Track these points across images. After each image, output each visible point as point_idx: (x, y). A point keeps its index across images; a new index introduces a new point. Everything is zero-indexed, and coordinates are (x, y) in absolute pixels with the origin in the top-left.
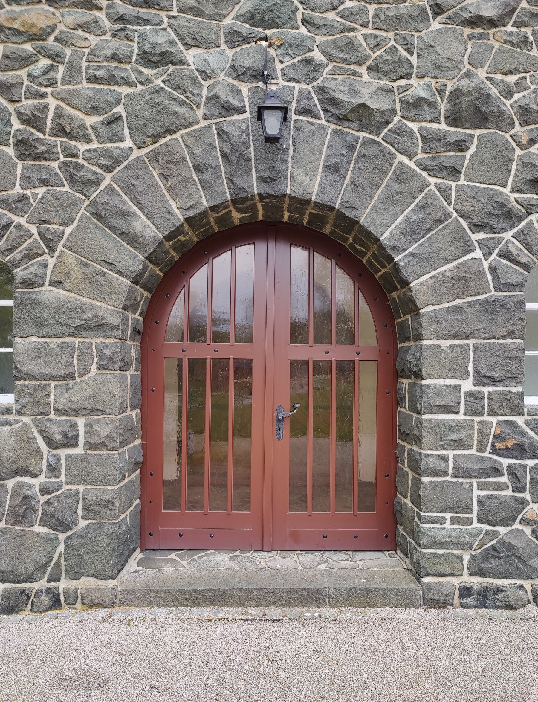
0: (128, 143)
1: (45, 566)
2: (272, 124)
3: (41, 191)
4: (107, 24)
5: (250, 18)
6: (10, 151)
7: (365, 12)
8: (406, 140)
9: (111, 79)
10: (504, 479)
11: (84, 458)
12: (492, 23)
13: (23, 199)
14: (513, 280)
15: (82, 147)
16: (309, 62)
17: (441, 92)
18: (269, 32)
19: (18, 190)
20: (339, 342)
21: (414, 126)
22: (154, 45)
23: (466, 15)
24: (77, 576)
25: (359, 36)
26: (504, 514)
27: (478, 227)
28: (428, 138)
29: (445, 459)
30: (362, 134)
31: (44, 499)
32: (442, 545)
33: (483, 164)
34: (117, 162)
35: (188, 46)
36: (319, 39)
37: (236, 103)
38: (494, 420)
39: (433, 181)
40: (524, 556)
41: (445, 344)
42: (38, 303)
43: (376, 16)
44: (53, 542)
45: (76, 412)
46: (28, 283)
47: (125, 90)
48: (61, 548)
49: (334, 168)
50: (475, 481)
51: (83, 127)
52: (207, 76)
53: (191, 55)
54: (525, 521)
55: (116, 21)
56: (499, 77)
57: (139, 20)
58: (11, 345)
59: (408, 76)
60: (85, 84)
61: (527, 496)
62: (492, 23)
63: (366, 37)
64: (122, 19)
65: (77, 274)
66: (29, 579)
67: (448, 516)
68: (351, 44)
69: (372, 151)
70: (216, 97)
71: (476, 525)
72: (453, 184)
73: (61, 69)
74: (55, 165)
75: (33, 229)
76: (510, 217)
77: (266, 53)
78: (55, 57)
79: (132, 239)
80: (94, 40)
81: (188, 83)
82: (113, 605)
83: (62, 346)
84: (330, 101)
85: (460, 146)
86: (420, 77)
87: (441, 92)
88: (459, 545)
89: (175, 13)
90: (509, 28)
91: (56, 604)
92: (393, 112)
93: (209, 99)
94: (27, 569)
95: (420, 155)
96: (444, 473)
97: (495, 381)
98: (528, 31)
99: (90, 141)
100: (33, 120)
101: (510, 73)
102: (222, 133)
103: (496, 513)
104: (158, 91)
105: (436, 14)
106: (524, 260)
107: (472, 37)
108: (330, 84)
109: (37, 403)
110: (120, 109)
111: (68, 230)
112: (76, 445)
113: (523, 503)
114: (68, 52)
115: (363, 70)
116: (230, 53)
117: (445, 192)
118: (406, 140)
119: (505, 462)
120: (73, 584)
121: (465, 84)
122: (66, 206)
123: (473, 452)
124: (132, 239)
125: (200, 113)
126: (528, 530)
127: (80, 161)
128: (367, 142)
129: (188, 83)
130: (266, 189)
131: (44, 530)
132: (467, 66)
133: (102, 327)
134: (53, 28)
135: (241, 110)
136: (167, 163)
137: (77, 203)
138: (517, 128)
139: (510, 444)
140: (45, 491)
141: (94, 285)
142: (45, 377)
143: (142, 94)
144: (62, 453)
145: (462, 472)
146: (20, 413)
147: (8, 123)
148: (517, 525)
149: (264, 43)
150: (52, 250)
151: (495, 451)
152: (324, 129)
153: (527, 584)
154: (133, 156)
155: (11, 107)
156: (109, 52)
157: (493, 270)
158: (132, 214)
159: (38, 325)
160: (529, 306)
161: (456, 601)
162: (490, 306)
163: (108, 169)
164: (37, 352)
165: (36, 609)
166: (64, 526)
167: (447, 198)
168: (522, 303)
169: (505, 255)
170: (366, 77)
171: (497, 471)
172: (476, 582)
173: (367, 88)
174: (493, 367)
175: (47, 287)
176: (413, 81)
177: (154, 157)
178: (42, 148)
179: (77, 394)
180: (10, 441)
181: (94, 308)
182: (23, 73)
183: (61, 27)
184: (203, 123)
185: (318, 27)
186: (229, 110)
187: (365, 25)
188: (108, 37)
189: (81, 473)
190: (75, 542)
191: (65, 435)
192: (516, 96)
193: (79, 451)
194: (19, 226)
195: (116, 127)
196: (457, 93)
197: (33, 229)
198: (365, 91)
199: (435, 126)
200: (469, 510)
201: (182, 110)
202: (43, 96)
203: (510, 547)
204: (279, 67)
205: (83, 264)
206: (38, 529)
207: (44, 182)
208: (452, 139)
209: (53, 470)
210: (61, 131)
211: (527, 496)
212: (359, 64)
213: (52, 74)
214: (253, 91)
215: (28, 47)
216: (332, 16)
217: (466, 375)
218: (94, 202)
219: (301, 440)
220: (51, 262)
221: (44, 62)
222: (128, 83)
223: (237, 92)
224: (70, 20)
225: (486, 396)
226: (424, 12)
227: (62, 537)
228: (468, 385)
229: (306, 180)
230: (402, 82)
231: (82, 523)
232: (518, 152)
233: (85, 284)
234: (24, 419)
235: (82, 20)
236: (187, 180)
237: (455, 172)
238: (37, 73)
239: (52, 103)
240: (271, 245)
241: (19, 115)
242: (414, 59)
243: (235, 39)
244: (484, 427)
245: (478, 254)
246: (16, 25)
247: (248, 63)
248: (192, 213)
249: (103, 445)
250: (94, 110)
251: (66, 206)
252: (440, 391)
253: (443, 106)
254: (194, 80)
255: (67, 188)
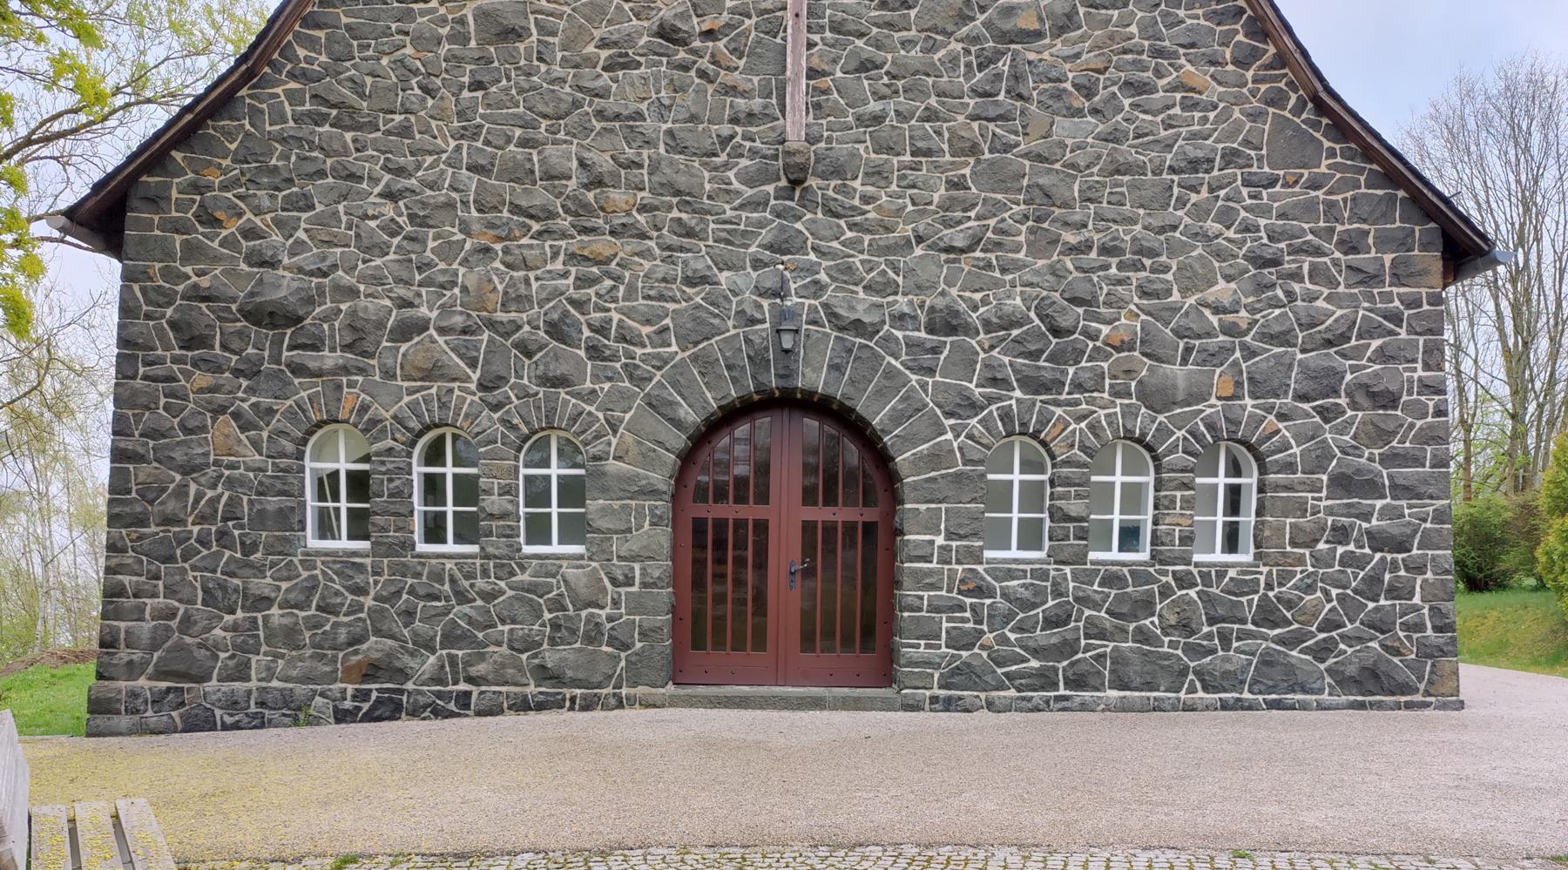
0: (674, 348)
1: (611, 677)
2: (787, 342)
3: (607, 386)
4: (657, 251)
5: (770, 247)
6: (582, 353)
7: (861, 241)
8: (892, 345)
9: (661, 298)
10: (968, 614)
11: (639, 595)
12: (962, 251)
13: (594, 391)
14: (976, 457)
15: (639, 351)
16: (816, 282)
17: (921, 306)
18: (785, 258)
19: (588, 384)
20: (845, 505)
21: (899, 334)
22: (695, 271)
23: (942, 244)
24: (635, 685)
25: (856, 261)
26: (965, 641)
27: (949, 415)
28: (912, 345)
29: (921, 598)
30: (858, 340)
31: (609, 626)
32: (917, 664)
33: (954, 364)
34: (666, 363)
35: (721, 270)
36: (825, 264)
37: (759, 316)
38: (960, 568)
39: (914, 377)
40: (979, 671)
41: (923, 507)
42: (604, 474)
43: (870, 245)
44: (617, 659)
45: (633, 559)
46: (596, 458)
47: (671, 306)
48: (623, 663)
49: (836, 368)
50: (944, 616)
51: (640, 336)
52: (736, 295)
53: (723, 277)
54: (982, 647)
55: (664, 250)
56: (968, 294)
57: (682, 249)
58: (583, 506)
59: (896, 293)
60: (641, 301)
61: (985, 628)
62: (962, 251)
63: (862, 262)
64: (669, 248)
65: (634, 450)
66: (599, 686)
67: (922, 642)
68: (849, 269)
69: (865, 354)
70: (743, 311)
71: (944, 649)
72: (930, 381)
73: (622, 288)
74: (618, 365)
75: (600, 415)
76: (974, 407)
77: (783, 276)
78: (618, 279)
79: (677, 423)
80: (647, 265)
81: (721, 300)
82: (663, 706)
83: (622, 507)
84: (833, 316)
85: (936, 350)
86: (905, 294)
87: (921, 306)
88: (928, 664)
89: (710, 243)
90: (978, 254)
91: (620, 705)
92: (884, 322)
93: (737, 313)
94: (597, 678)
95: (904, 358)
96: (921, 610)
97: (961, 537)
98: (992, 256)
99: (644, 346)
100: (601, 330)
101: (976, 291)
102: (748, 341)
103: (960, 641)
104: (699, 307)
105: (918, 243)
106: (984, 441)
107: (947, 261)
108: (833, 301)
109: (603, 551)
110: (667, 321)
111: (628, 416)
112: (632, 585)
113: (982, 633)
114: (627, 274)
115: (859, 289)
116: (754, 275)
117: (924, 386)
118: (892, 345)
119: (968, 601)
120: (632, 691)
121: (941, 303)
122: (627, 397)
123: (944, 593)
124: (677, 423)
125: (730, 323)
126: (985, 654)
127: (637, 362)
128: (863, 346)
129: (721, 300)
130: (782, 383)
131: (610, 650)
132: (943, 286)
133: (653, 493)
134: (615, 255)
135: (763, 321)
136: (705, 363)
137: (636, 395)
138: (982, 335)
139: (971, 586)
140: (610, 619)
141: (647, 460)
142: (610, 531)
143: (686, 310)
144: (623, 590)
145: (933, 608)
146: (590, 559)
147: (581, 332)
148: (976, 650)
149: (781, 267)
150: (615, 432)
151: (960, 592)
152: (828, 335)
153: (983, 695)
154: (678, 358)
155: (582, 319)
156: (660, 276)
157: (960, 449)
158: (678, 404)
159: (604, 491)
160: (990, 477)
161: (927, 706)
162: (958, 476)
163: (659, 369)
164: (604, 511)
165: (606, 707)
166: (626, 646)
167: (926, 391)
168: (983, 475)
169: (970, 437)
170: (862, 295)
171: (962, 608)
172: (943, 693)
173: (861, 305)
174: (960, 526)
175: (611, 461)
176: (899, 298)
177: (695, 358)
178: (608, 352)
179: (634, 544)
180: (584, 580)
181: (647, 477)
182: (591, 291)
183: (621, 254)
184: (733, 332)
185: (824, 254)
186: (753, 321)
187: (862, 252)
188: (658, 262)
189: (636, 606)
190: (633, 659)
191: (626, 576)
192: (982, 310)
193: (635, 589)
194: (590, 413)
195: (665, 335)
196: (932, 309)
197: (600, 415)
198: (860, 307)
199: (916, 334)
200: (938, 637)
201: (716, 321)
202: (608, 310)
203: (968, 665)
204: (793, 286)
205: (639, 443)
206: (605, 648)
207: (610, 379)
208: (928, 345)
209: (616, 603)
210: (622, 338)
211: (985, 628)
212: (856, 284)
213: (614, 293)
214: (772, 305)
215: (595, 270)
216: (835, 244)
217: (938, 532)
218: (648, 394)
219: (809, 583)
220: (614, 441)
221: (608, 283)
222: (674, 300)
223: (759, 307)
224: (628, 248)
225: (122, 636)
226: (909, 241)
227: (623, 655)
228: (940, 540)
229: (814, 377)
230: (890, 299)
231: (639, 645)
232: (982, 355)
233: (640, 458)
234: (594, 564)
235: (638, 249)
236: (721, 376)
237: (931, 371)
238: (603, 292)
239: (616, 317)
240: (786, 413)
241: (590, 326)
242: (900, 280)
243: (758, 264)
244: (952, 572)
245: (949, 436)
246: (586, 253)
247: (768, 284)
248: (724, 402)
249: (654, 585)
250: (648, 322)
251: (627, 397)
252: (918, 544)
253: (923, 318)
254: (726, 298)
255: (627, 384)
